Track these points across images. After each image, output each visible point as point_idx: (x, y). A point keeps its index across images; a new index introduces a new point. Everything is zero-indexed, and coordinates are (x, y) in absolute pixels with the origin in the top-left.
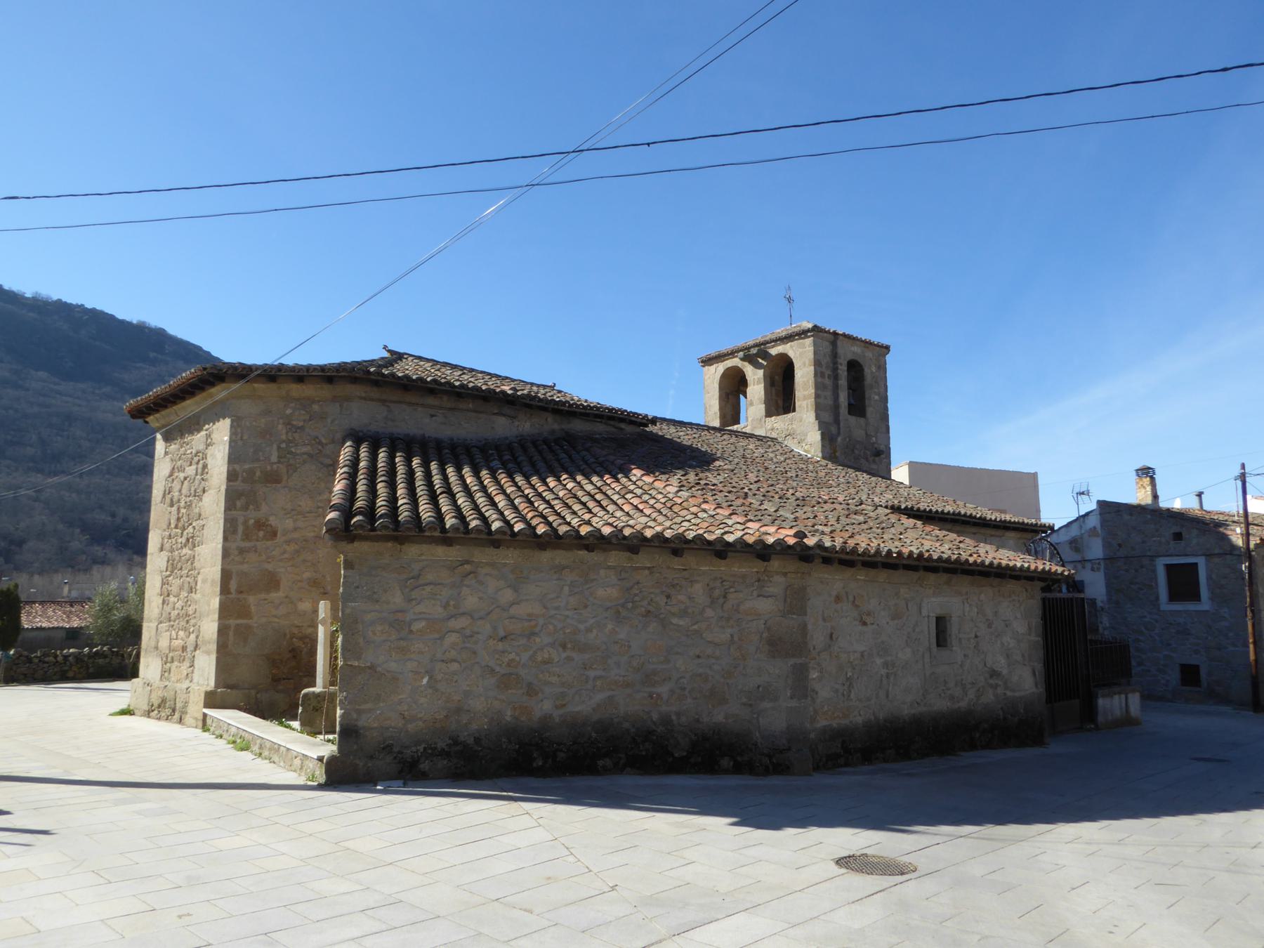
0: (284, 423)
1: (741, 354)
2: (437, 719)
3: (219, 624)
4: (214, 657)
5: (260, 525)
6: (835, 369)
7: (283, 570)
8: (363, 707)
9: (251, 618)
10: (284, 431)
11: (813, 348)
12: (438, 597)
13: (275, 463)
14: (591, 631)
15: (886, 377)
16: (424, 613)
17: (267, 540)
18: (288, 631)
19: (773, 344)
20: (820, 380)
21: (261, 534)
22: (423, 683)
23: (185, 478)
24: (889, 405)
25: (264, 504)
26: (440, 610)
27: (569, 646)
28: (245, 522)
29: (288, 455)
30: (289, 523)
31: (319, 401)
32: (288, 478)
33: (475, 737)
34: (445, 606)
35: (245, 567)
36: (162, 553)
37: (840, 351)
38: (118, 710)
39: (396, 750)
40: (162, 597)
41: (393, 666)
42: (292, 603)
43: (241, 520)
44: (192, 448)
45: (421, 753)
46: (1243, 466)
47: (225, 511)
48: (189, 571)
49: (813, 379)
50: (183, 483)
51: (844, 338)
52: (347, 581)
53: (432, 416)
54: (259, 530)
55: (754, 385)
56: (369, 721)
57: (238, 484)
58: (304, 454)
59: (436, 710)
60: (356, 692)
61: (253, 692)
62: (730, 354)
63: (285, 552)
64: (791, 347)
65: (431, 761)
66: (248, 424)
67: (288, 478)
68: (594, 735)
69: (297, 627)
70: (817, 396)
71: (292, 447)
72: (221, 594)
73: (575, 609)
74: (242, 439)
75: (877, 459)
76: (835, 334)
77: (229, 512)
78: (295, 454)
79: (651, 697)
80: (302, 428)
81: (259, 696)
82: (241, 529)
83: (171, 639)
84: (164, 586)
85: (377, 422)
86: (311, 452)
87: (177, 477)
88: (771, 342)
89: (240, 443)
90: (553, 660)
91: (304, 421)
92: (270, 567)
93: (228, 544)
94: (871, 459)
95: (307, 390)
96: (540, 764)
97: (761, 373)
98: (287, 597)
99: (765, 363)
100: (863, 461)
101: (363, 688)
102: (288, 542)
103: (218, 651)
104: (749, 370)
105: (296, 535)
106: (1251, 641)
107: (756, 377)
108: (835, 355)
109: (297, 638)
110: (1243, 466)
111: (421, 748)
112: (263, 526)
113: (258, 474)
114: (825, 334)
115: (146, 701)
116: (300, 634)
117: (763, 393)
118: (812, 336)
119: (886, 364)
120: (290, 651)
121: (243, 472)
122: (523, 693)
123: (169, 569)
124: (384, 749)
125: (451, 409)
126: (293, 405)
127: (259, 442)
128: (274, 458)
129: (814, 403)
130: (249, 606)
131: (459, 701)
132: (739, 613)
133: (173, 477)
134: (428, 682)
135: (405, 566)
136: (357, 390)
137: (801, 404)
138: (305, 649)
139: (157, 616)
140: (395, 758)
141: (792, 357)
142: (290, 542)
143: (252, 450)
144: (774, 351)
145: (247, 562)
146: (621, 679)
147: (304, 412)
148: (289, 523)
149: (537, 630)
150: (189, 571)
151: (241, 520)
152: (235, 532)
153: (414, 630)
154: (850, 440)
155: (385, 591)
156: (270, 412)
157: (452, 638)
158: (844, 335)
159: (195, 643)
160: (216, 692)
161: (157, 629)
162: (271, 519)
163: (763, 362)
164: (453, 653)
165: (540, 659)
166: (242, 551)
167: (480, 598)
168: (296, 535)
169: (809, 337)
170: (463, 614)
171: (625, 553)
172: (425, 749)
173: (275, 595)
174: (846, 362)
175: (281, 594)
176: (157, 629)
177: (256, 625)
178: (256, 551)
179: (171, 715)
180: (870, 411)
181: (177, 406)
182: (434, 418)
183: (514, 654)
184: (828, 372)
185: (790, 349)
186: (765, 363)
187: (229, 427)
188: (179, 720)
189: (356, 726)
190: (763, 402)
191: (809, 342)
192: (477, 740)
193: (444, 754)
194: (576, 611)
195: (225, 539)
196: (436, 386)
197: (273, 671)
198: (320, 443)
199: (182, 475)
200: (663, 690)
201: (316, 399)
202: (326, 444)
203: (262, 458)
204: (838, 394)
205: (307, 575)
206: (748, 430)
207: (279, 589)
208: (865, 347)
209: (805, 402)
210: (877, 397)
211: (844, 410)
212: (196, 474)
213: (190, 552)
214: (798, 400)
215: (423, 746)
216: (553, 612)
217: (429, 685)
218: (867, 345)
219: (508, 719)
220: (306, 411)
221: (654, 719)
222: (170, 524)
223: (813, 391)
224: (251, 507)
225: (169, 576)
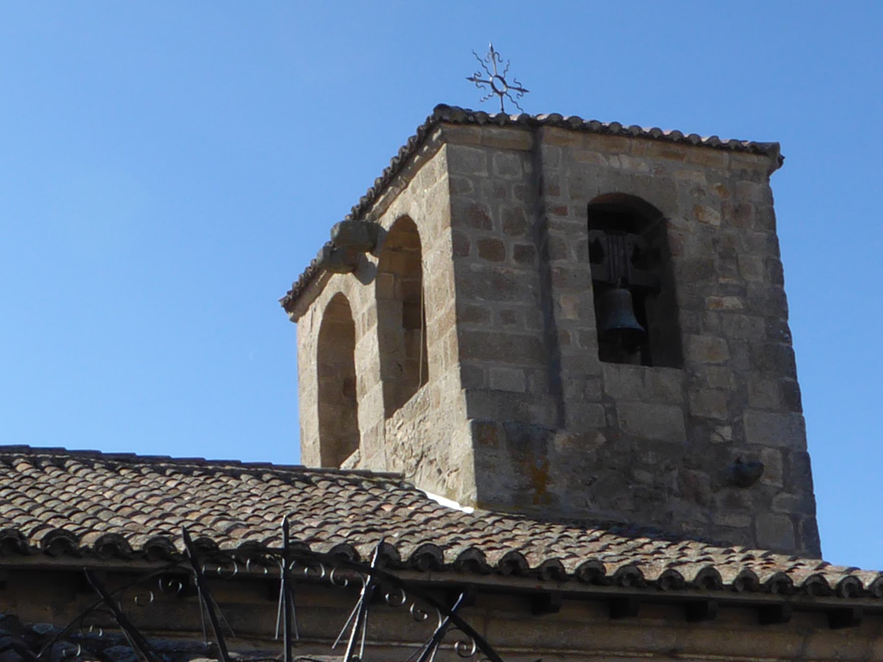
20: (477, 266)
75: (746, 495)
76: (529, 124)
94: (719, 497)
100: (676, 505)
114: (495, 131)
154: (608, 443)
158: (555, 121)
204: (552, 301)
206: (378, 466)
208: (665, 154)
210: (731, 302)
218: (674, 148)
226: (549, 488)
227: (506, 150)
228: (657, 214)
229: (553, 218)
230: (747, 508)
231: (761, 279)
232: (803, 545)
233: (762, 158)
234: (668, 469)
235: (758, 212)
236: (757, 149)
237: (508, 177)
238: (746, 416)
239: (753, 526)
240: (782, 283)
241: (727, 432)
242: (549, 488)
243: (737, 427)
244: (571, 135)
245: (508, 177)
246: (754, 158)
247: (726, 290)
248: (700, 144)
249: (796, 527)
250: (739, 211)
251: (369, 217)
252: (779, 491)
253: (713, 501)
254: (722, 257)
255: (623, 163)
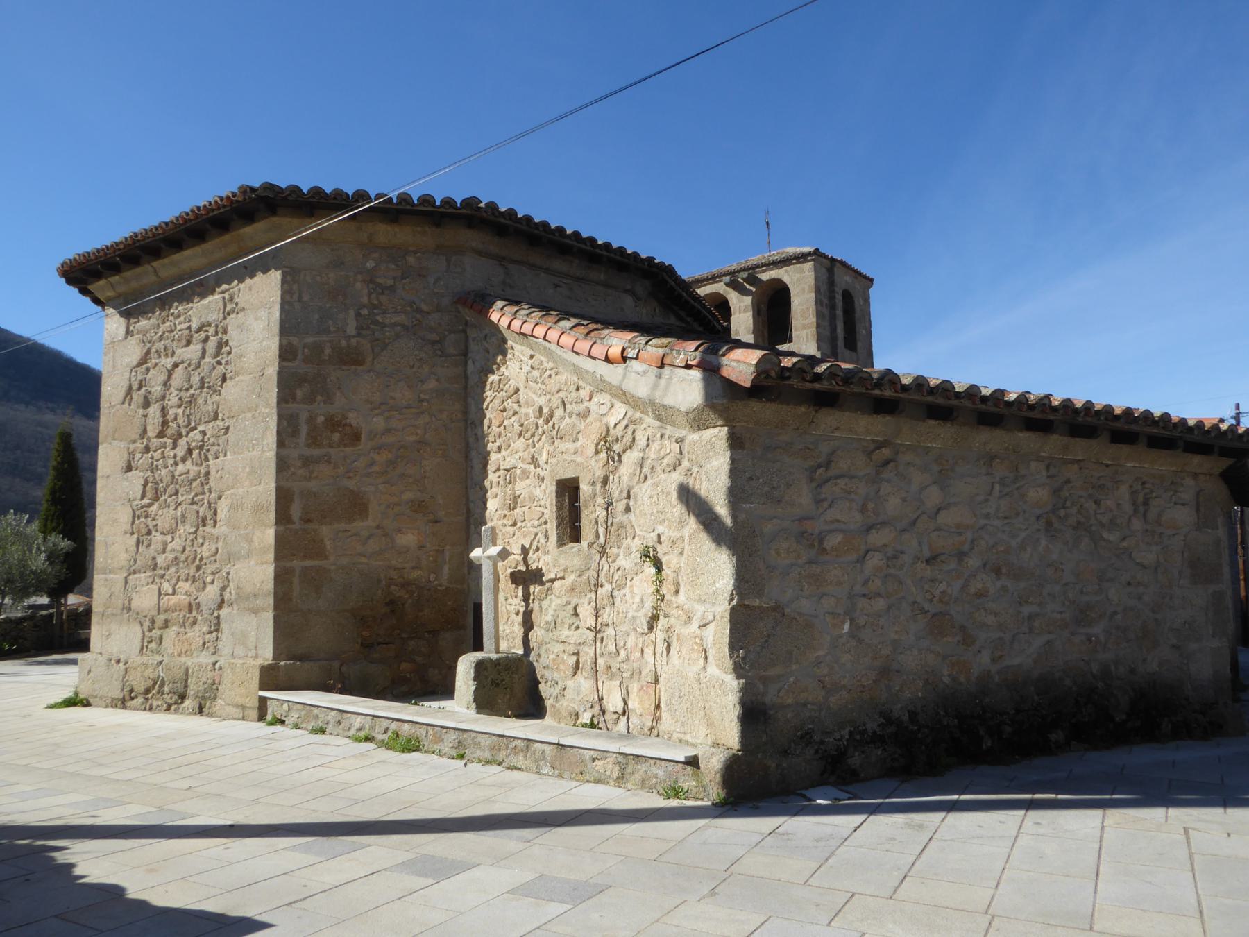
0: (364, 281)
1: (726, 279)
2: (864, 686)
3: (276, 567)
4: (268, 617)
5: (334, 424)
6: (832, 298)
7: (372, 489)
8: (772, 672)
9: (326, 558)
10: (365, 291)
11: (813, 273)
12: (853, 496)
13: (354, 337)
14: (1025, 550)
15: (870, 312)
16: (838, 521)
17: (346, 446)
18: (382, 576)
19: (764, 268)
21: (336, 436)
22: (844, 631)
23: (176, 365)
24: (873, 341)
25: (338, 394)
26: (858, 516)
27: (1004, 571)
28: (311, 420)
29: (372, 326)
30: (379, 423)
31: (415, 252)
32: (374, 359)
33: (909, 711)
34: (863, 509)
35: (313, 485)
36: (129, 474)
37: (837, 278)
38: (60, 700)
39: (817, 738)
40: (136, 536)
41: (806, 605)
42: (386, 535)
43: (303, 417)
44: (190, 321)
45: (847, 740)
46: (1238, 407)
47: (278, 403)
48: (196, 495)
49: (814, 307)
50: (170, 373)
51: (840, 266)
52: (736, 468)
53: (556, 286)
54: (332, 432)
55: (740, 313)
56: (781, 694)
57: (298, 365)
58: (395, 324)
59: (863, 672)
60: (758, 649)
61: (336, 664)
62: (710, 279)
63: (373, 463)
64: (786, 272)
65: (863, 752)
66: (308, 279)
67: (374, 359)
68: (1036, 698)
69: (395, 569)
70: (818, 326)
71: (378, 314)
72: (277, 524)
73: (1006, 518)
74: (300, 300)
76: (833, 260)
77: (284, 405)
78: (383, 325)
79: (1090, 640)
80: (392, 289)
81: (344, 669)
82: (304, 430)
83: (160, 594)
84: (137, 522)
85: (493, 287)
86: (407, 324)
87: (156, 364)
88: (762, 266)
89: (297, 306)
90: (988, 592)
91: (394, 278)
92: (351, 484)
93: (285, 452)
95: (402, 234)
96: (989, 744)
97: (748, 300)
98: (378, 527)
99: (754, 290)
101: (766, 641)
102: (379, 449)
103: (277, 607)
104: (733, 297)
105: (390, 439)
106: (1242, 577)
107: (742, 305)
108: (831, 283)
109: (397, 585)
110: (1238, 407)
111: (846, 733)
112: (338, 426)
113: (328, 351)
115: (118, 685)
116: (401, 580)
117: (751, 321)
118: (813, 260)
119: (869, 298)
120: (387, 604)
121: (304, 348)
122: (959, 641)
123: (149, 495)
124: (802, 737)
125: (579, 279)
126: (376, 255)
127: (328, 306)
128: (351, 329)
129: (815, 333)
130: (322, 540)
131: (888, 656)
132: (1160, 525)
133: (149, 365)
134: (850, 629)
135: (811, 446)
136: (473, 238)
137: (799, 335)
138: (410, 601)
139: (125, 563)
140: (817, 752)
141: (788, 283)
142: (380, 448)
143: (317, 317)
144: (765, 276)
145: (317, 477)
146: (1059, 616)
147: (393, 266)
148: (379, 423)
149: (966, 548)
150: (196, 495)
151: (303, 417)
152: (295, 433)
153: (827, 548)
155: (788, 486)
156: (342, 263)
157: (875, 560)
159: (219, 598)
160: (279, 667)
161: (126, 583)
162: (351, 415)
163: (751, 288)
164: (877, 584)
165: (972, 590)
166: (307, 462)
167: (904, 500)
168: (390, 439)
169: (809, 261)
170: (883, 523)
171: (1065, 438)
172: (851, 733)
173: (361, 524)
174: (841, 291)
175: (370, 523)
176: (126, 583)
177: (333, 568)
178: (329, 462)
179: (176, 703)
180: (859, 345)
181: (161, 261)
182: (558, 289)
183: (944, 583)
184: (826, 301)
185: (785, 275)
186: (754, 290)
187: (279, 283)
188: (197, 710)
189: (764, 704)
190: (751, 331)
191: (808, 267)
192: (913, 715)
193: (877, 739)
194: (1006, 521)
195: (281, 443)
196: (575, 243)
197: (364, 633)
198: (419, 311)
199: (168, 362)
200: (1097, 630)
201: (411, 249)
202: (428, 313)
203: (332, 329)
205: (407, 496)
207: (367, 517)
209: (805, 332)
211: (841, 343)
212: (203, 356)
213: (196, 468)
214: (796, 330)
215: (848, 729)
216: (983, 522)
217: (852, 635)
219: (946, 680)
220: (397, 265)
221: (1095, 671)
222: (145, 431)
223: (814, 320)
224: (319, 398)
225: (149, 505)
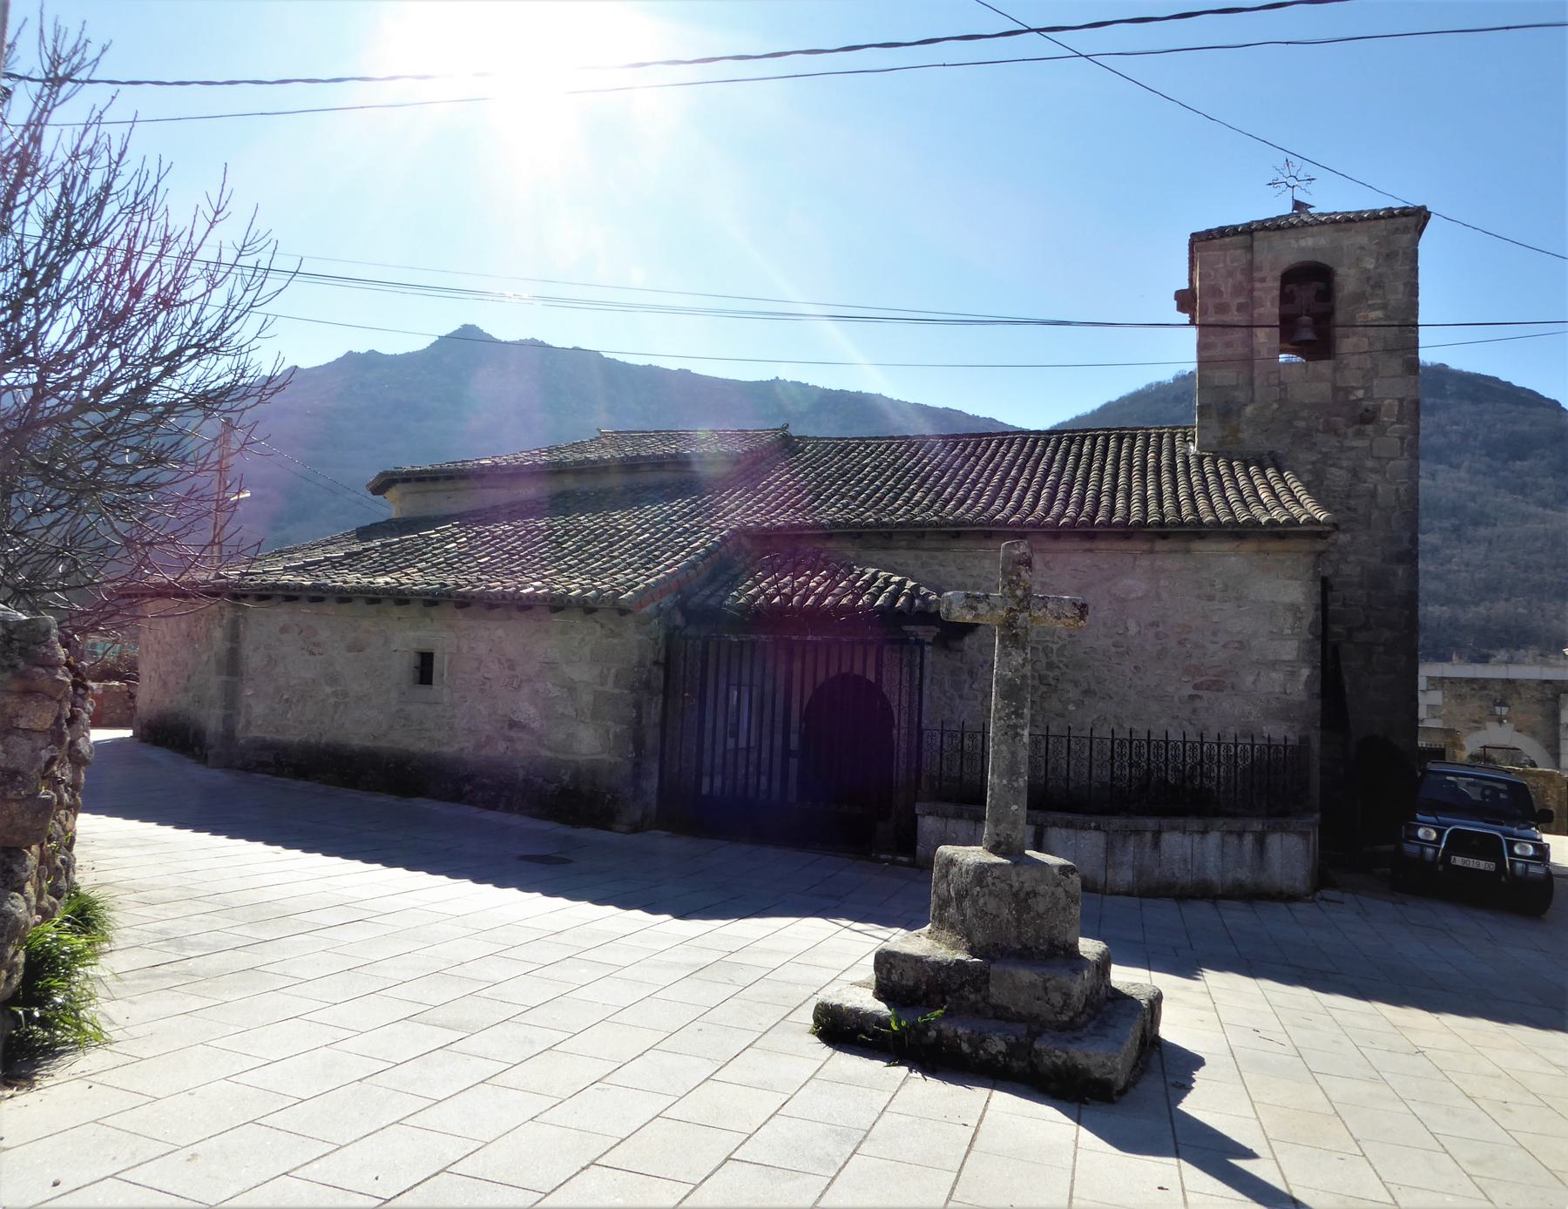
75: (1369, 428)
94: (1350, 431)
226: (1240, 435)
227: (1236, 248)
228: (1331, 269)
229: (1258, 285)
230: (1368, 435)
231: (1400, 296)
232: (1406, 454)
233: (1410, 218)
234: (1317, 418)
235: (1404, 253)
236: (1405, 212)
237: (1236, 264)
238: (1375, 382)
239: (1371, 445)
240: (1417, 296)
241: (1360, 394)
242: (1240, 435)
243: (1368, 389)
244: (1272, 233)
245: (1236, 264)
246: (1404, 219)
247: (1372, 308)
248: (1362, 220)
249: (1402, 443)
250: (1390, 257)
251: (45, 620)
252: (1393, 423)
253: (1345, 434)
254: (1373, 287)
255: (1308, 242)
